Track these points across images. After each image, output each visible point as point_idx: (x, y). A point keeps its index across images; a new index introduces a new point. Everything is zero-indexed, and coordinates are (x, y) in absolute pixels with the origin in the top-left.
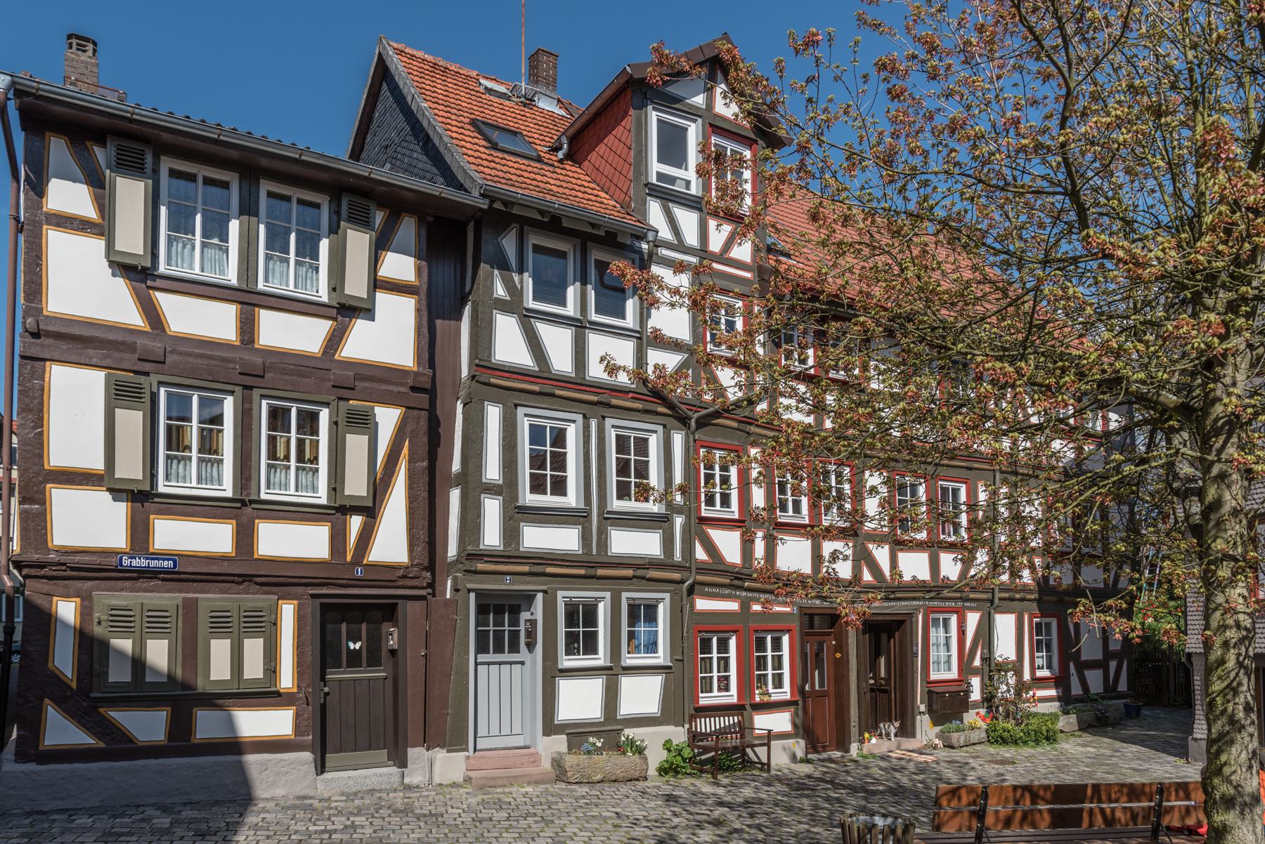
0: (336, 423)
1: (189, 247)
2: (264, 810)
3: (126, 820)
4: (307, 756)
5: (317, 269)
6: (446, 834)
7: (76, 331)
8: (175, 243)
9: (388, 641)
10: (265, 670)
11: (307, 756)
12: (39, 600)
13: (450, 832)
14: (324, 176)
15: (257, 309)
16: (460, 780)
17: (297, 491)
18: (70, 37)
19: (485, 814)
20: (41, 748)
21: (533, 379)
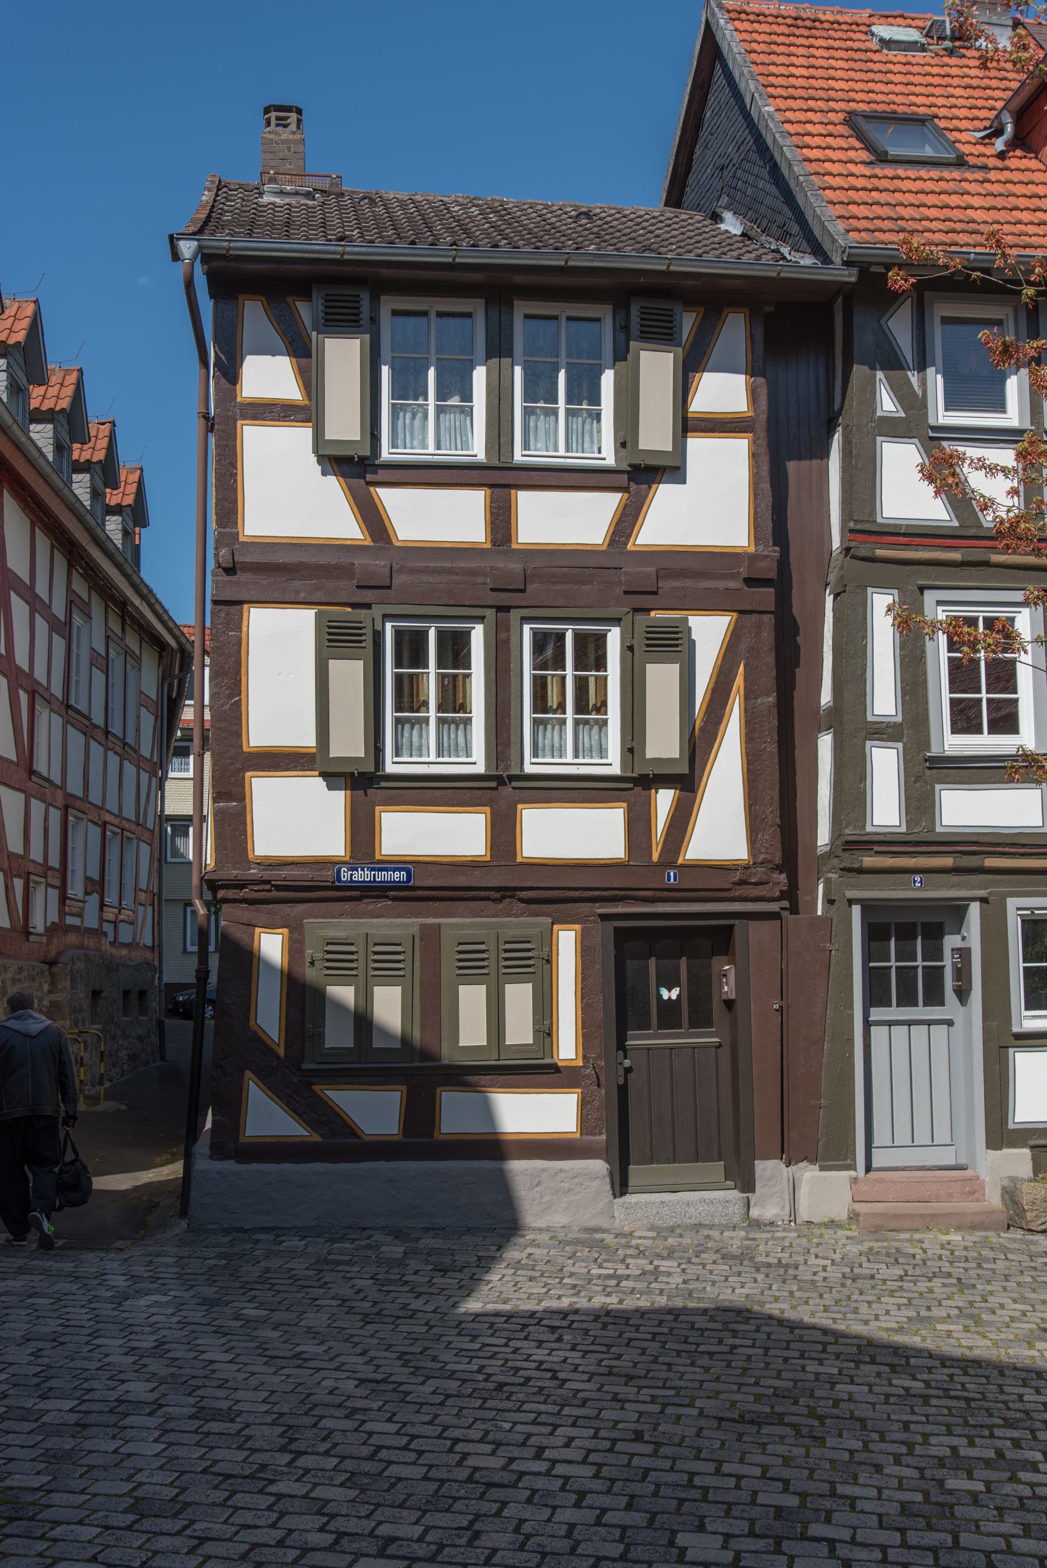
0: (631, 648)
1: (419, 416)
2: (534, 1243)
3: (347, 1245)
4: (598, 1166)
5: (598, 417)
6: (791, 1293)
7: (279, 558)
8: (401, 414)
9: (721, 987)
10: (536, 1032)
11: (598, 1166)
12: (238, 933)
13: (800, 1289)
14: (605, 282)
15: (513, 492)
16: (843, 1216)
17: (576, 756)
18: (267, 110)
19: (867, 1268)
20: (242, 1140)
21: (949, 542)
